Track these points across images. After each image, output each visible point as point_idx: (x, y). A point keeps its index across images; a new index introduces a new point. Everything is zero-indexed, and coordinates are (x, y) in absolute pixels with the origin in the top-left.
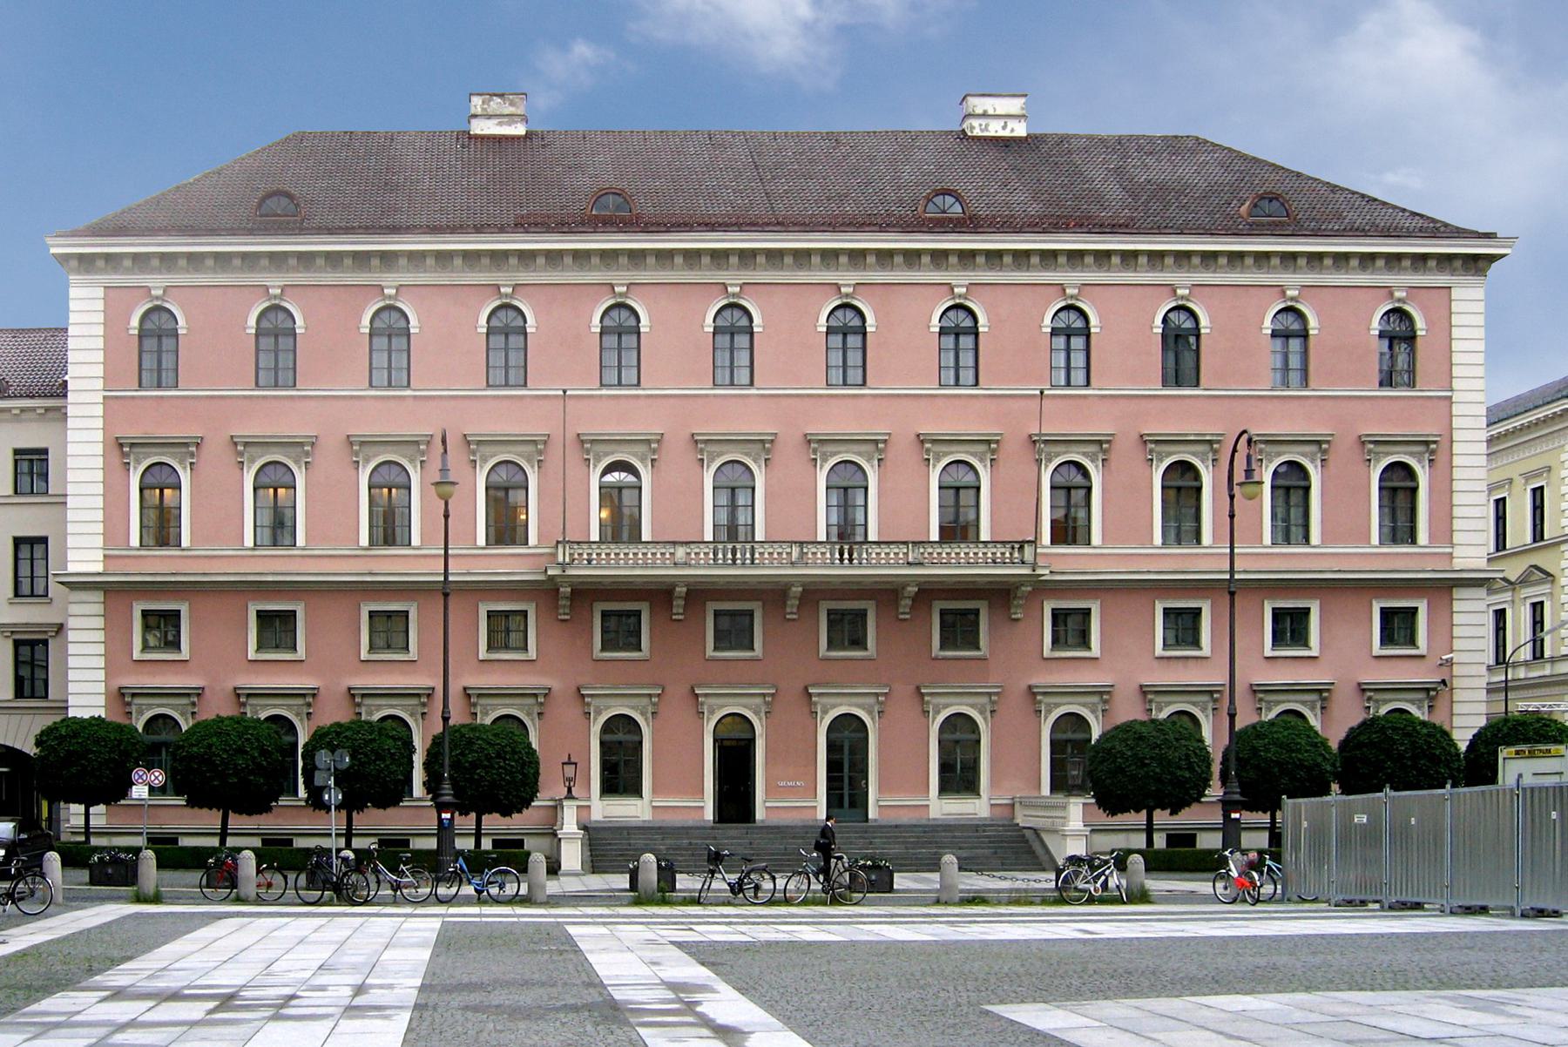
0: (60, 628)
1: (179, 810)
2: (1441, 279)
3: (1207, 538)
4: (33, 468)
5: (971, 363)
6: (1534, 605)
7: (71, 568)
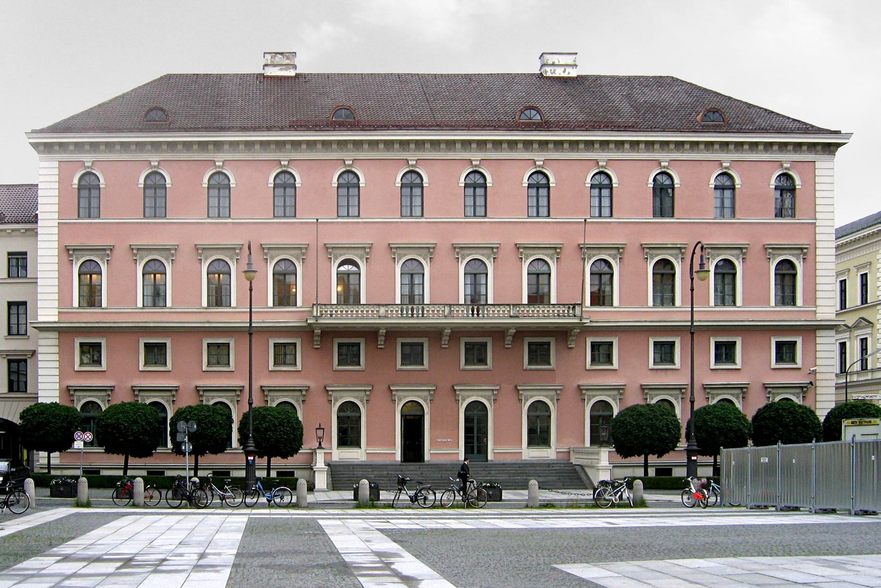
0: (34, 353)
1: (101, 455)
2: (810, 157)
3: (678, 302)
4: (18, 263)
5: (546, 204)
6: (862, 340)
7: (40, 319)
